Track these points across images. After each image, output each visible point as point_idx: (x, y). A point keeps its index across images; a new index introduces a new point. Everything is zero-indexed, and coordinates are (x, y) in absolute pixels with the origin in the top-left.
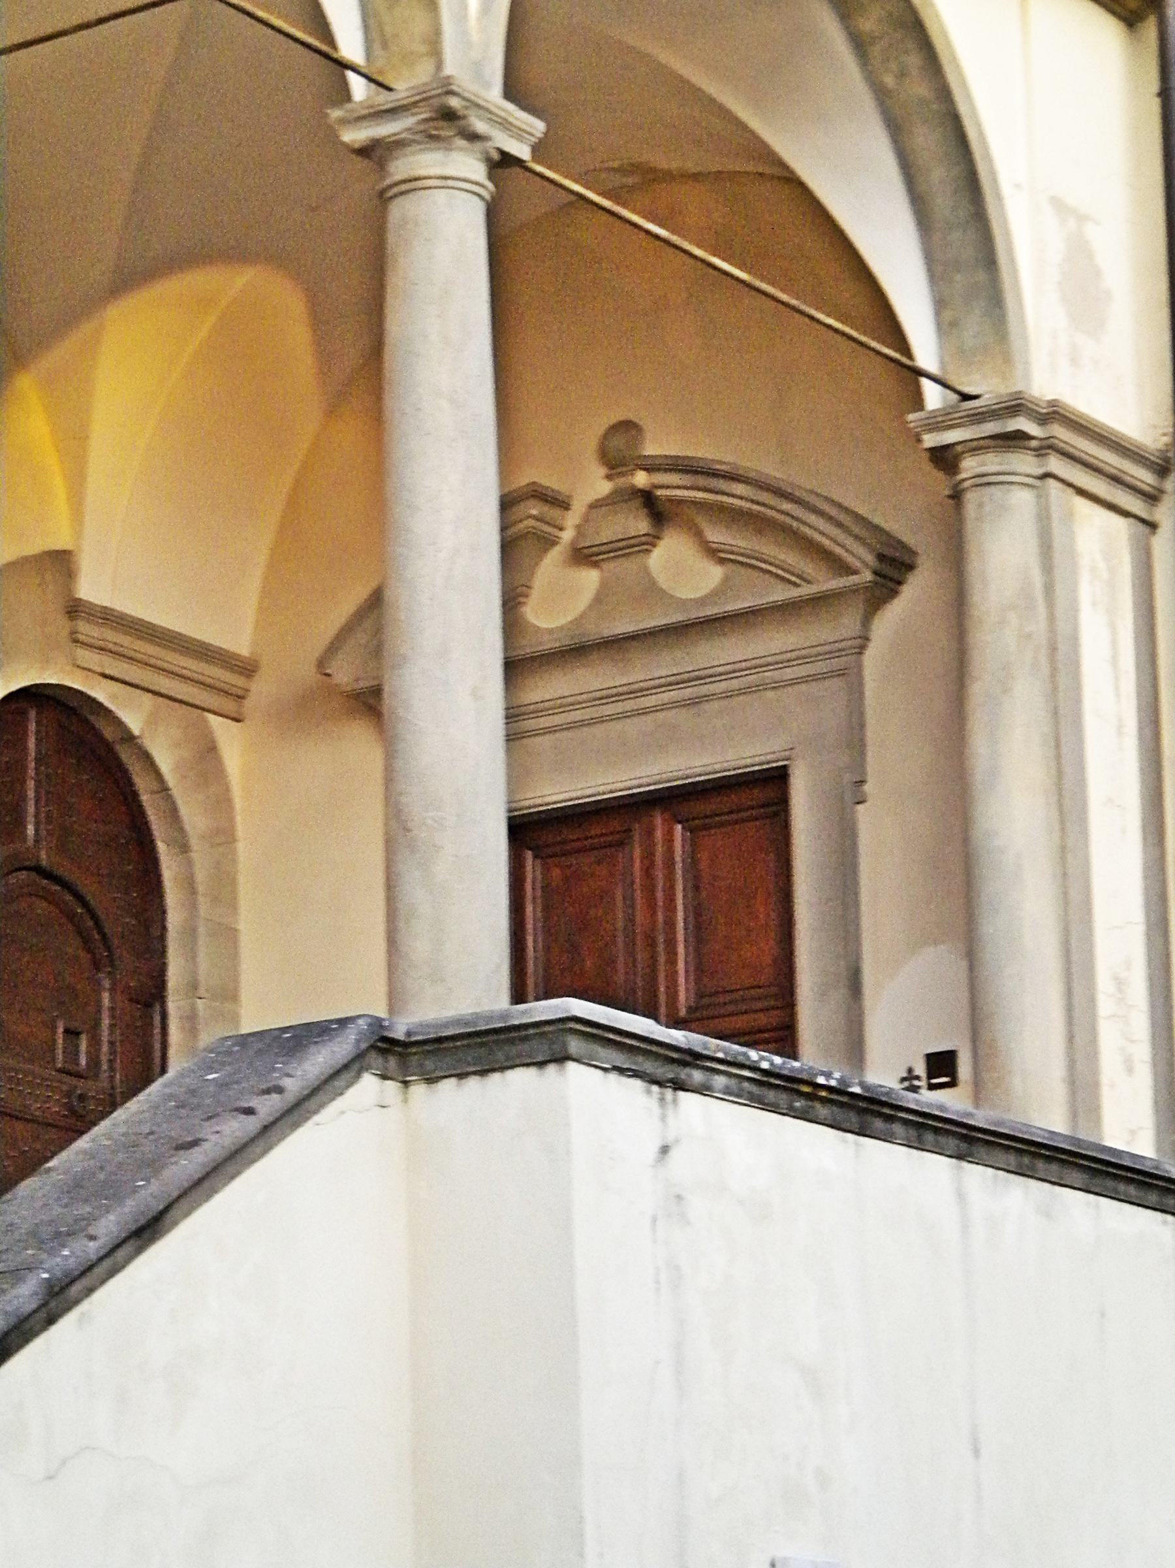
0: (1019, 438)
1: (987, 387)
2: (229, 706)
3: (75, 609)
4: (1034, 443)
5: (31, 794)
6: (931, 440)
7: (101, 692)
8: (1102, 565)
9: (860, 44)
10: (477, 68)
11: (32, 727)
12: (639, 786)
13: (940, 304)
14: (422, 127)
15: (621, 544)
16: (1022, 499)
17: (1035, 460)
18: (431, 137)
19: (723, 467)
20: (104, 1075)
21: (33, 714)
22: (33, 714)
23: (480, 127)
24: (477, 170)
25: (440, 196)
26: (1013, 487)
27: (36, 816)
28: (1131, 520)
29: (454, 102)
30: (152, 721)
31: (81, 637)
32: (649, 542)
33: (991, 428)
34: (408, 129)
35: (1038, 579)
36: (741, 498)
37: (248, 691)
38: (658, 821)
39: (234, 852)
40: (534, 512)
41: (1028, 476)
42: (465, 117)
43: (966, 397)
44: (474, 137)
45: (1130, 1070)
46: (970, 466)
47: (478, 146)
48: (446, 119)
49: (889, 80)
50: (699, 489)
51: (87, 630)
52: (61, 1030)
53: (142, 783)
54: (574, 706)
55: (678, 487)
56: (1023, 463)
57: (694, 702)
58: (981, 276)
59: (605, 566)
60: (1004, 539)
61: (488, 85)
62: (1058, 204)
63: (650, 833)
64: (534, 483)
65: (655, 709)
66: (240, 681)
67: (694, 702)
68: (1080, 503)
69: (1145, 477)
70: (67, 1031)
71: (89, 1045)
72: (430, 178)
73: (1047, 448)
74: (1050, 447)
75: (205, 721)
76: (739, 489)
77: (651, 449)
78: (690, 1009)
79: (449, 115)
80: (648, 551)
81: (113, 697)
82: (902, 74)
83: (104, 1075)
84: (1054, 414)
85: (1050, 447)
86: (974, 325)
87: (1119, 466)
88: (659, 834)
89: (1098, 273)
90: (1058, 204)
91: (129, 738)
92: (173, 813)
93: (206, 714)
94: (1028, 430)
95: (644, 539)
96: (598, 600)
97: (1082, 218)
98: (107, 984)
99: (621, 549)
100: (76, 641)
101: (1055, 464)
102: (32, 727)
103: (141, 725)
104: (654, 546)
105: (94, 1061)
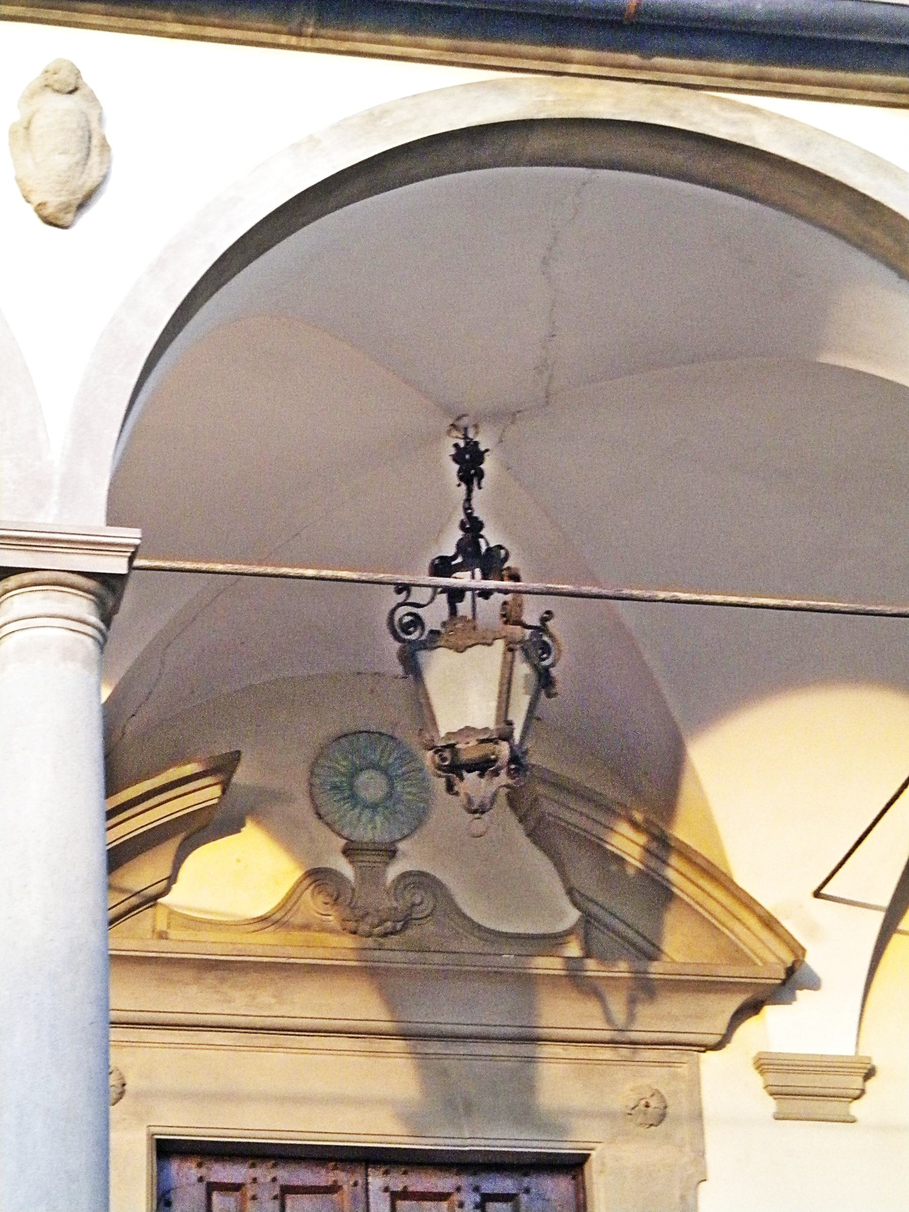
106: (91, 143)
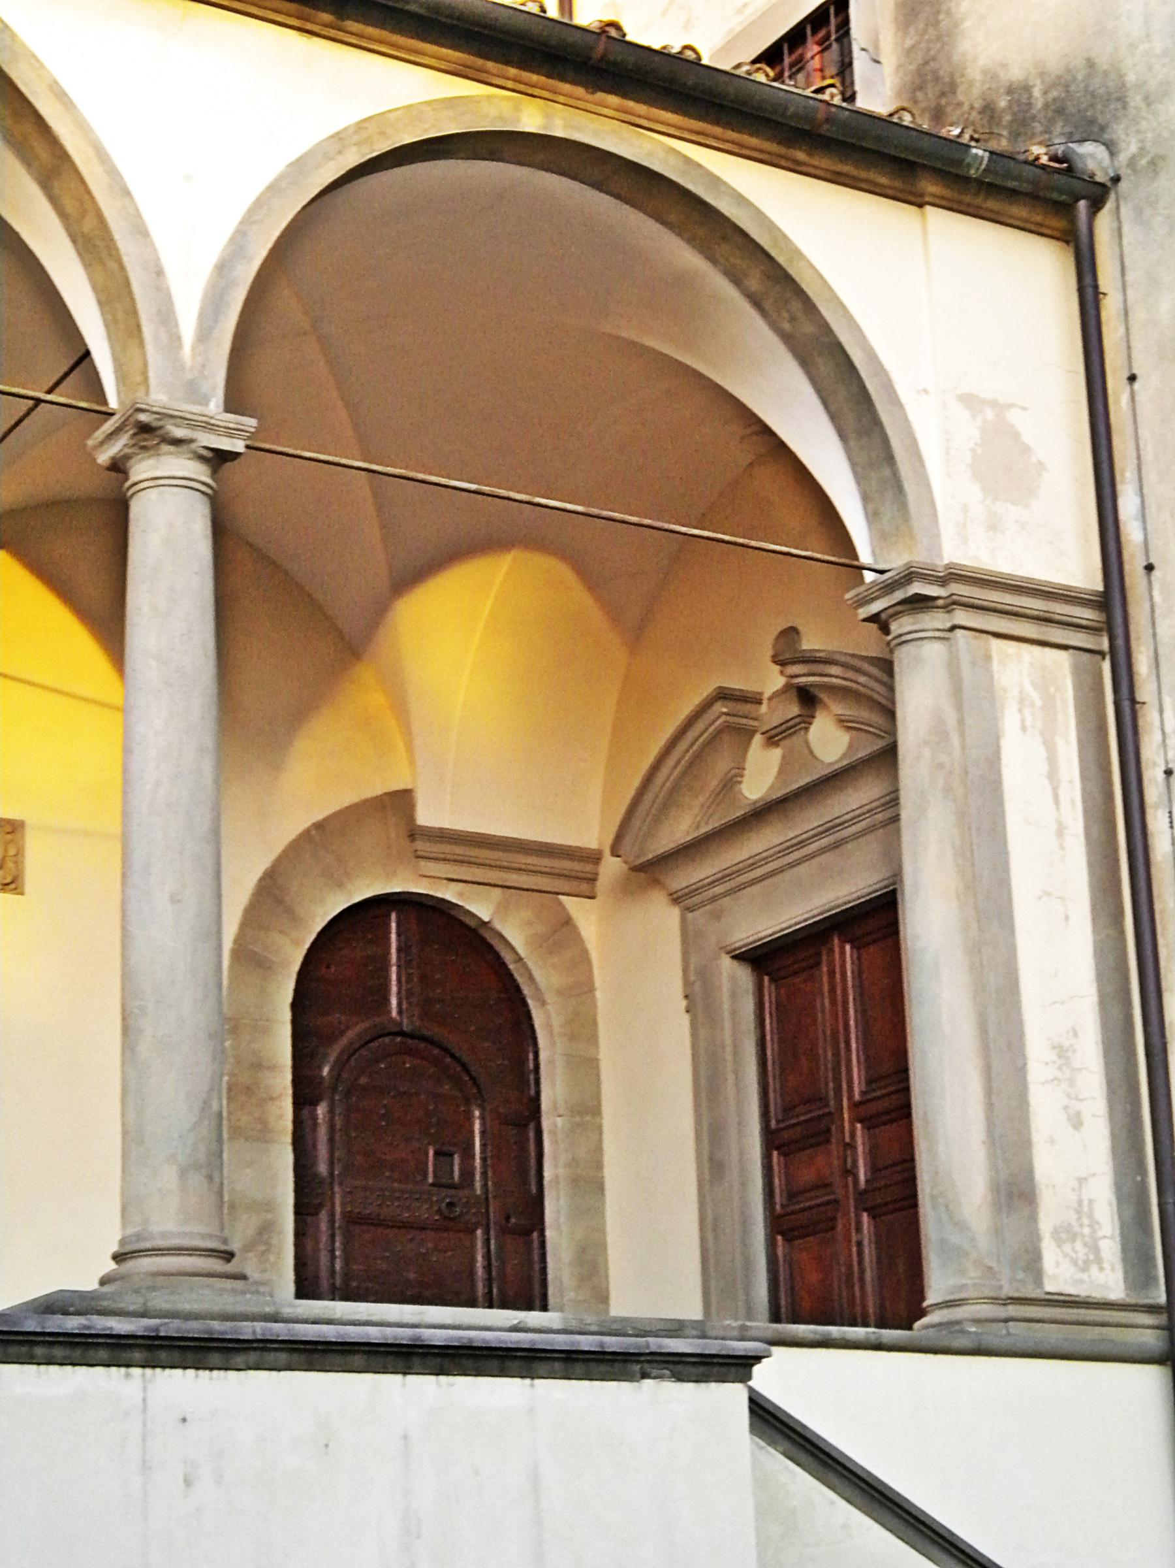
0: (920, 603)
1: (896, 561)
2: (584, 887)
3: (415, 833)
4: (940, 602)
5: (394, 977)
6: (864, 612)
7: (449, 893)
8: (1034, 695)
9: (757, 303)
10: (193, 390)
11: (394, 925)
12: (814, 917)
13: (866, 498)
14: (133, 442)
15: (784, 727)
16: (933, 652)
17: (946, 615)
18: (144, 448)
19: (821, 655)
20: (478, 1185)
21: (393, 916)
22: (393, 916)
23: (179, 433)
24: (200, 472)
25: (153, 494)
26: (925, 641)
27: (399, 993)
28: (1071, 651)
29: (143, 417)
30: (502, 908)
31: (419, 853)
32: (806, 720)
33: (899, 595)
34: (125, 445)
35: (951, 717)
36: (837, 677)
37: (597, 874)
38: (836, 941)
39: (594, 998)
40: (725, 710)
41: (939, 630)
42: (161, 428)
43: (882, 572)
44: (177, 442)
45: (1077, 1122)
46: (895, 627)
47: (184, 448)
48: (149, 433)
49: (786, 326)
50: (814, 675)
51: (422, 846)
52: (431, 1153)
53: (508, 958)
54: (766, 860)
55: (804, 675)
56: (935, 620)
57: (836, 846)
58: (887, 472)
59: (782, 743)
60: (921, 692)
61: (205, 401)
62: (969, 401)
63: (832, 950)
64: (720, 687)
65: (812, 856)
66: (588, 868)
67: (836, 846)
68: (996, 643)
69: (1087, 615)
70: (437, 1153)
71: (462, 1160)
72: (141, 481)
73: (952, 604)
74: (954, 603)
75: (560, 903)
76: (834, 670)
77: (806, 645)
78: (862, 1093)
79: (145, 429)
80: (807, 729)
81: (461, 895)
82: (793, 319)
83: (478, 1185)
84: (953, 575)
85: (954, 603)
86: (888, 511)
87: (1045, 609)
88: (837, 949)
89: (1026, 450)
90: (969, 401)
91: (485, 924)
92: (531, 978)
93: (560, 897)
94: (921, 595)
95: (797, 720)
96: (781, 771)
97: (1000, 407)
98: (477, 1113)
99: (784, 731)
100: (418, 857)
101: (961, 617)
102: (394, 925)
103: (490, 913)
104: (810, 724)
105: (467, 1173)
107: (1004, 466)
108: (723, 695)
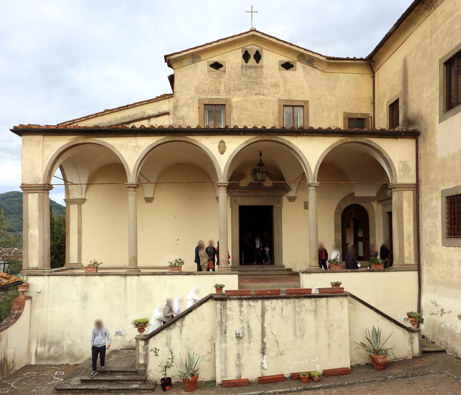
73: (398, 188)
106: (225, 147)
107: (405, 169)
108: (384, 184)
